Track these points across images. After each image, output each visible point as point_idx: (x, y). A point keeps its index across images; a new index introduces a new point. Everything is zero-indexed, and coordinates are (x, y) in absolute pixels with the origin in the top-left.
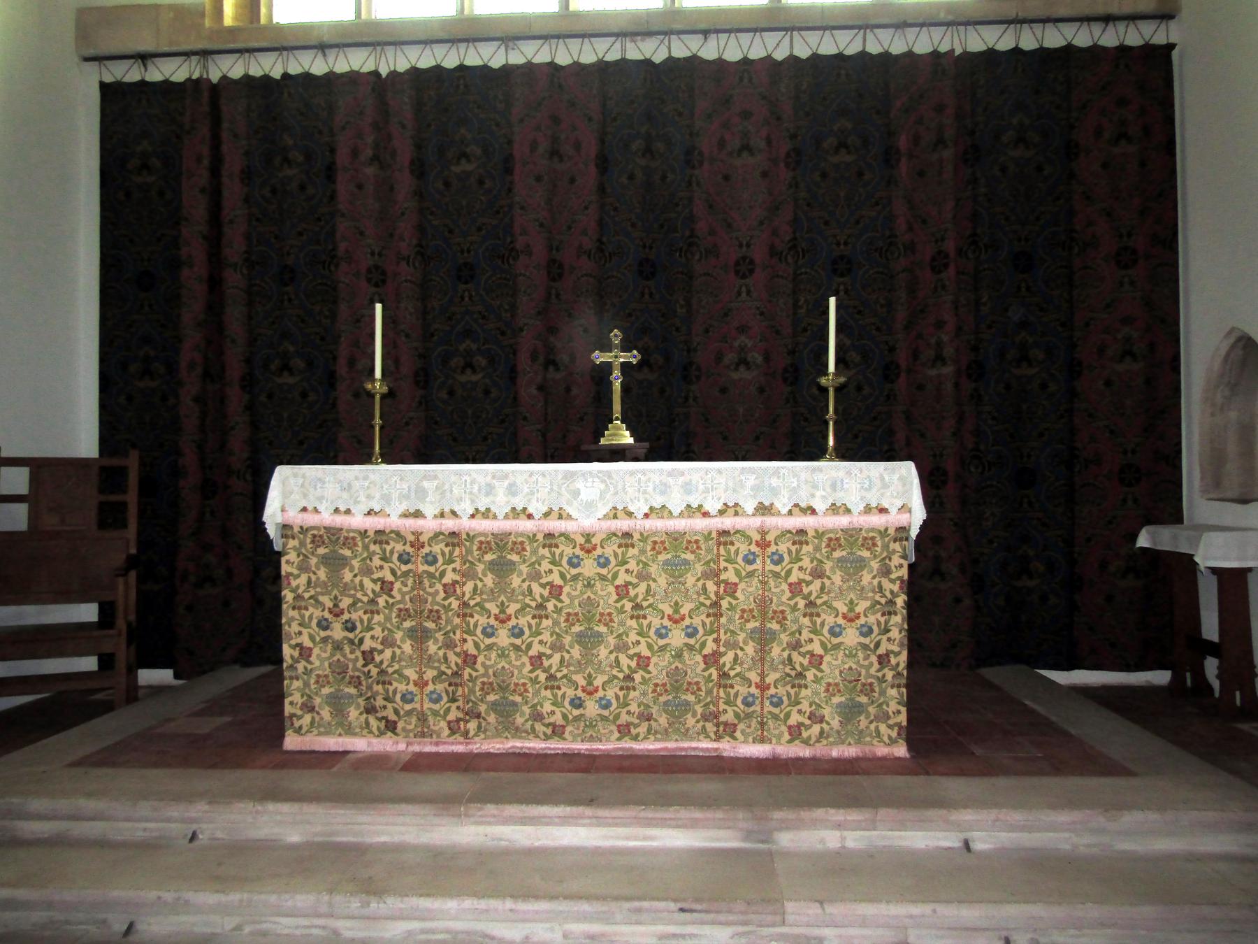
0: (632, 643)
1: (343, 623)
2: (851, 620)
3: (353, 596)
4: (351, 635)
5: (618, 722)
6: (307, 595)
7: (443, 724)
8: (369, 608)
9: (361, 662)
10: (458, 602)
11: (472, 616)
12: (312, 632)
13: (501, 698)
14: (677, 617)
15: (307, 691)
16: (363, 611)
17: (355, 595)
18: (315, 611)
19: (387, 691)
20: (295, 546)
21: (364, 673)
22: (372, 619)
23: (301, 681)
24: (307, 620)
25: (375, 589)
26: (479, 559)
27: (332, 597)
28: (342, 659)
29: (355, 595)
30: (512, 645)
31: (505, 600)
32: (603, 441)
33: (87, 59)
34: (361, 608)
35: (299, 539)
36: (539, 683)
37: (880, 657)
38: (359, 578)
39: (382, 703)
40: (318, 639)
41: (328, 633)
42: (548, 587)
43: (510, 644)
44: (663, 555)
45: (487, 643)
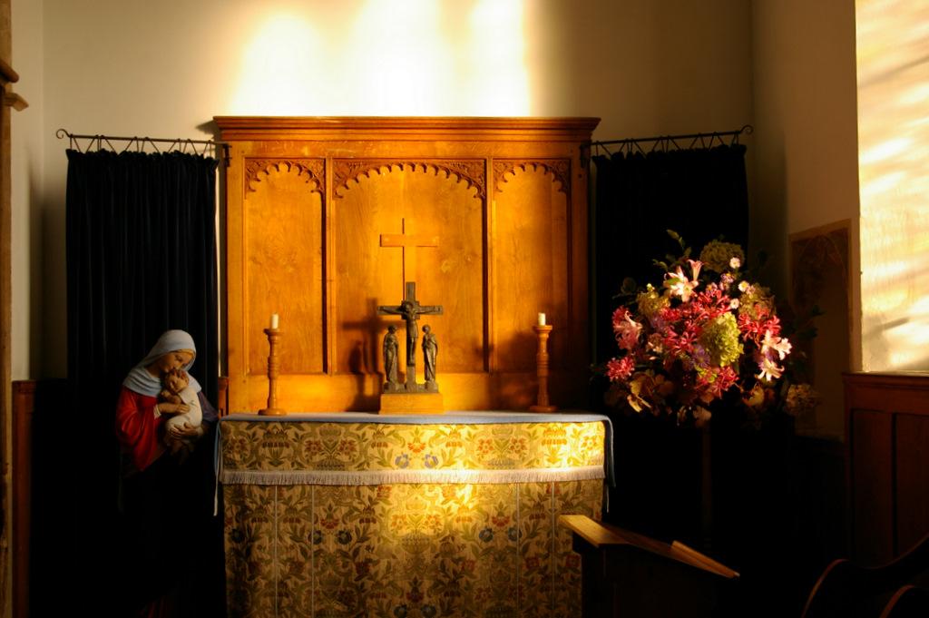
0: (459, 547)
1: (336, 535)
2: (330, 527)
3: (349, 505)
6: (299, 507)
9: (355, 574)
10: (561, 502)
16: (358, 520)
17: (351, 503)
20: (289, 455)
21: (357, 587)
23: (567, 592)
24: (298, 534)
25: (372, 496)
26: (308, 461)
28: (503, 570)
29: (351, 503)
30: (339, 551)
32: (680, 268)
35: (294, 447)
36: (534, 585)
37: (359, 565)
40: (480, 550)
42: (376, 489)
44: (317, 455)
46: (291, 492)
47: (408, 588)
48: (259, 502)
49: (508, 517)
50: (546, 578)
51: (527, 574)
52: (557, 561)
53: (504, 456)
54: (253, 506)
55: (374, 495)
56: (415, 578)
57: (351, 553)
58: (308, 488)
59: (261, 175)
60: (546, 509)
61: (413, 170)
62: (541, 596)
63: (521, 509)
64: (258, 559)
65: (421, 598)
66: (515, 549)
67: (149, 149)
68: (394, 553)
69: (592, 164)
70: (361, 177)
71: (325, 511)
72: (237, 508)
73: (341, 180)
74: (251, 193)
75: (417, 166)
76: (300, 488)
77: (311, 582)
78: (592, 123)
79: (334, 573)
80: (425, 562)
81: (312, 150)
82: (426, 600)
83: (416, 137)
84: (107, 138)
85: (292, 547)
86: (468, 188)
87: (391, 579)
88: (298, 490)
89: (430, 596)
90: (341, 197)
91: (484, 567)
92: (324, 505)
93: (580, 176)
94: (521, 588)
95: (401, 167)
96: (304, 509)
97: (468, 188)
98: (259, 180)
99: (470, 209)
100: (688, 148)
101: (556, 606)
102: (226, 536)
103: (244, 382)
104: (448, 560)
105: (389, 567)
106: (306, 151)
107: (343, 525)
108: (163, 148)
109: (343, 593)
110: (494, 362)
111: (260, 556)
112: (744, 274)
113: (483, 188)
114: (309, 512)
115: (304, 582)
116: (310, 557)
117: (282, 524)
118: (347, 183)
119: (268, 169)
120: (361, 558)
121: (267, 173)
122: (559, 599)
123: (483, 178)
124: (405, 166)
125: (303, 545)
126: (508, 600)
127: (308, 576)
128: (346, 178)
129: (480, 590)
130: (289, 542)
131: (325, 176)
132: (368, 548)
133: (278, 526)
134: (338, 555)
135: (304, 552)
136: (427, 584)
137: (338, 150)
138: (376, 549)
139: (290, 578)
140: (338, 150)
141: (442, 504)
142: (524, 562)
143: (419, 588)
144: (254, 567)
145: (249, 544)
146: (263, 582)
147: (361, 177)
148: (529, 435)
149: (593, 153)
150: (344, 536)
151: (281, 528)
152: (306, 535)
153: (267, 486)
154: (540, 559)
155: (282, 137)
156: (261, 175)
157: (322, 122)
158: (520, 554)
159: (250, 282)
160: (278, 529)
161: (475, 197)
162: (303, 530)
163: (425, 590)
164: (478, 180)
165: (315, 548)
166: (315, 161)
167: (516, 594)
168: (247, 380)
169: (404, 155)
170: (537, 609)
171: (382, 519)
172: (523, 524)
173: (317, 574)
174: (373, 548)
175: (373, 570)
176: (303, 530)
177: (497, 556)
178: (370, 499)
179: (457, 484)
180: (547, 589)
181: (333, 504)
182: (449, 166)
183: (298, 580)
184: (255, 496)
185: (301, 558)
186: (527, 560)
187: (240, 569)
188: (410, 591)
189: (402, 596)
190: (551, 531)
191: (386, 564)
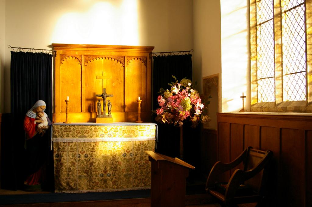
3: (88, 147)
5: (135, 160)
7: (111, 182)
19: (96, 174)
27: (81, 148)
30: (85, 159)
33: (243, 93)
37: (90, 163)
38: (112, 161)
39: (95, 177)
41: (125, 157)
47: (104, 169)
48: (63, 147)
51: (135, 165)
52: (143, 161)
54: (62, 148)
55: (94, 145)
57: (88, 160)
58: (76, 143)
59: (64, 59)
62: (138, 170)
65: (107, 172)
67: (34, 52)
69: (153, 59)
70: (92, 60)
73: (86, 61)
77: (77, 168)
81: (78, 53)
82: (108, 172)
85: (72, 159)
89: (109, 171)
90: (86, 66)
93: (149, 61)
94: (133, 169)
95: (102, 58)
96: (76, 148)
98: (64, 61)
101: (143, 173)
105: (98, 164)
106: (77, 53)
107: (86, 153)
108: (38, 51)
109: (86, 171)
110: (126, 109)
112: (192, 87)
114: (77, 149)
117: (69, 152)
120: (91, 161)
121: (66, 59)
127: (76, 166)
128: (88, 60)
129: (123, 169)
130: (71, 157)
131: (82, 60)
135: (75, 160)
136: (108, 168)
139: (71, 167)
144: (62, 164)
146: (64, 168)
147: (92, 60)
149: (153, 55)
152: (76, 155)
155: (70, 49)
162: (75, 154)
164: (123, 62)
165: (78, 159)
170: (138, 174)
171: (97, 151)
175: (94, 164)
176: (75, 154)
181: (83, 147)
185: (75, 162)
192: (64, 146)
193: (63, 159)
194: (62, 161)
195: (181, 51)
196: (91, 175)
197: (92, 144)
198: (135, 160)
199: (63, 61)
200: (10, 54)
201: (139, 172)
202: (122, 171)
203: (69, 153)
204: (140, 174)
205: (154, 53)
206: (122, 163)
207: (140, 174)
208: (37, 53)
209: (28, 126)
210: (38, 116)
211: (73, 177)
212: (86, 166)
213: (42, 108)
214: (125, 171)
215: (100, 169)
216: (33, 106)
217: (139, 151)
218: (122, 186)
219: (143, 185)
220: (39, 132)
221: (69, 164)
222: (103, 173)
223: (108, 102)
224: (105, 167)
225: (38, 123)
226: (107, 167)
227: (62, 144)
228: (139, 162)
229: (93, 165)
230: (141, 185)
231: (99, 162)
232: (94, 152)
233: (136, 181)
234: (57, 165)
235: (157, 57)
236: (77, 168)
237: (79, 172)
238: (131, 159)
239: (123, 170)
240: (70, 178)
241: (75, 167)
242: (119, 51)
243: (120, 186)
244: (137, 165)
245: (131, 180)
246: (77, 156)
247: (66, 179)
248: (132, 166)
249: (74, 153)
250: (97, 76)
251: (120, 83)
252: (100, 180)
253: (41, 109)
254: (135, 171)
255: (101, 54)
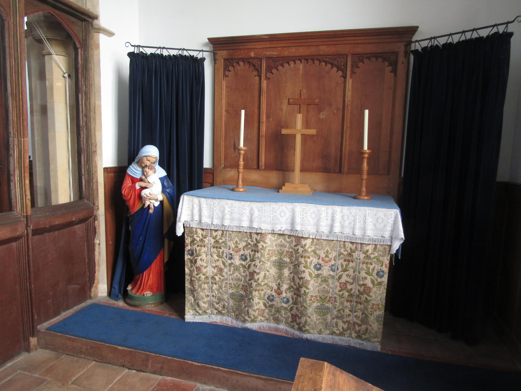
1: (240, 256)
4: (244, 263)
8: (347, 258)
10: (364, 255)
11: (309, 258)
12: (373, 278)
13: (321, 305)
14: (327, 259)
15: (366, 312)
18: (377, 266)
21: (295, 250)
22: (348, 265)
25: (257, 238)
28: (326, 287)
30: (241, 264)
31: (238, 240)
34: (249, 249)
36: (343, 298)
37: (250, 273)
40: (314, 275)
41: (320, 272)
42: (259, 235)
43: (240, 264)
45: (379, 281)
46: (216, 233)
47: (276, 287)
48: (201, 237)
49: (331, 259)
50: (351, 295)
51: (340, 291)
52: (358, 287)
53: (239, 292)
54: (198, 239)
55: (259, 238)
56: (279, 283)
57: (247, 266)
58: (225, 232)
59: (231, 68)
60: (354, 257)
61: (307, 63)
62: (346, 304)
63: (339, 255)
64: (200, 265)
65: (282, 294)
66: (334, 276)
67: (165, 53)
68: (268, 269)
69: (412, 57)
70: (280, 68)
71: (234, 244)
72: (191, 239)
73: (269, 69)
74: (226, 78)
75: (309, 60)
76: (221, 232)
77: (227, 279)
78: (413, 30)
79: (239, 275)
80: (285, 275)
81: (255, 54)
82: (284, 295)
83: (309, 44)
84: (143, 47)
85: (218, 260)
86: (337, 72)
87: (266, 282)
88: (220, 233)
89: (286, 293)
90: (269, 79)
91: (315, 284)
92: (233, 241)
93: (403, 63)
94: (335, 298)
95: (301, 61)
96: (223, 242)
97: (337, 72)
98: (230, 71)
99: (337, 83)
100: (470, 38)
101: (355, 312)
102: (186, 252)
103: (221, 171)
104: (296, 277)
105: (265, 276)
106: (252, 54)
107: (243, 252)
108: (173, 53)
109: (243, 286)
111: (201, 264)
113: (345, 72)
114: (226, 244)
115: (224, 278)
116: (227, 266)
117: (212, 248)
118: (273, 71)
119: (234, 65)
120: (251, 270)
121: (234, 67)
122: (357, 308)
123: (345, 66)
124: (303, 61)
125: (223, 260)
126: (327, 303)
127: (225, 275)
128: (272, 68)
129: (312, 296)
130: (216, 258)
131: (261, 68)
132: (254, 265)
133: (210, 250)
134: (241, 266)
135: (224, 264)
136: (285, 287)
137: (268, 53)
138: (258, 267)
139: (217, 275)
140: (268, 53)
141: (294, 246)
142: (338, 284)
143: (281, 288)
144: (198, 269)
145: (196, 258)
146: (203, 277)
147: (280, 68)
148: (249, 284)
149: (413, 48)
150: (243, 257)
151: (212, 251)
152: (225, 255)
153: (205, 229)
154: (348, 284)
155: (241, 47)
156: (231, 68)
157: (260, 37)
158: (336, 279)
159: (225, 122)
160: (210, 251)
161: (340, 77)
162: (223, 253)
163: (284, 290)
164: (342, 67)
165: (229, 262)
166: (257, 59)
167: (332, 300)
168: (222, 170)
169: (302, 54)
170: (344, 311)
171: (262, 251)
172: (340, 264)
173: (231, 275)
174: (257, 266)
175: (256, 277)
176: (223, 253)
177: (323, 279)
178: (256, 239)
179: (302, 237)
180: (351, 301)
181: (238, 240)
182: (327, 60)
183: (221, 277)
184: (199, 233)
185: (223, 267)
186: (340, 283)
187: (192, 269)
188: (276, 289)
189: (272, 291)
190: (356, 270)
191: (263, 274)
192: (202, 235)
193: (201, 260)
194: (199, 263)
195: (476, 27)
196: (250, 297)
197: (254, 236)
198: (340, 281)
199: (229, 72)
200: (128, 60)
201: (347, 307)
202: (311, 300)
203: (212, 250)
204: (349, 313)
205: (417, 41)
206: (312, 282)
207: (349, 313)
208: (172, 55)
209: (126, 191)
210: (145, 175)
211: (219, 295)
212: (242, 276)
213: (149, 161)
214: (317, 300)
215: (267, 286)
216: (136, 156)
217: (351, 264)
218: (368, 338)
219: (354, 335)
220: (144, 205)
221: (213, 269)
222: (274, 293)
223: (85, 119)
224: (279, 284)
225: (143, 188)
226: (281, 284)
227: (200, 232)
228: (349, 287)
229: (253, 277)
230: (351, 334)
231: (267, 273)
232: (258, 252)
233: (339, 324)
234: (190, 271)
235: (420, 49)
236: (226, 279)
237: (231, 287)
238: (333, 277)
239: (374, 307)
240: (215, 296)
241: (223, 276)
242: (332, 43)
243: (364, 337)
244: (344, 292)
245: (329, 320)
246: (226, 255)
247: (208, 296)
248: (333, 291)
249: (221, 251)
250: (289, 99)
251: (334, 114)
252: (268, 305)
253: (148, 162)
254: (338, 304)
255: (297, 54)
